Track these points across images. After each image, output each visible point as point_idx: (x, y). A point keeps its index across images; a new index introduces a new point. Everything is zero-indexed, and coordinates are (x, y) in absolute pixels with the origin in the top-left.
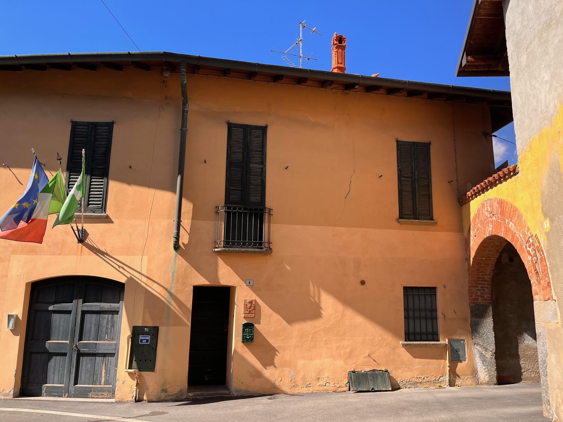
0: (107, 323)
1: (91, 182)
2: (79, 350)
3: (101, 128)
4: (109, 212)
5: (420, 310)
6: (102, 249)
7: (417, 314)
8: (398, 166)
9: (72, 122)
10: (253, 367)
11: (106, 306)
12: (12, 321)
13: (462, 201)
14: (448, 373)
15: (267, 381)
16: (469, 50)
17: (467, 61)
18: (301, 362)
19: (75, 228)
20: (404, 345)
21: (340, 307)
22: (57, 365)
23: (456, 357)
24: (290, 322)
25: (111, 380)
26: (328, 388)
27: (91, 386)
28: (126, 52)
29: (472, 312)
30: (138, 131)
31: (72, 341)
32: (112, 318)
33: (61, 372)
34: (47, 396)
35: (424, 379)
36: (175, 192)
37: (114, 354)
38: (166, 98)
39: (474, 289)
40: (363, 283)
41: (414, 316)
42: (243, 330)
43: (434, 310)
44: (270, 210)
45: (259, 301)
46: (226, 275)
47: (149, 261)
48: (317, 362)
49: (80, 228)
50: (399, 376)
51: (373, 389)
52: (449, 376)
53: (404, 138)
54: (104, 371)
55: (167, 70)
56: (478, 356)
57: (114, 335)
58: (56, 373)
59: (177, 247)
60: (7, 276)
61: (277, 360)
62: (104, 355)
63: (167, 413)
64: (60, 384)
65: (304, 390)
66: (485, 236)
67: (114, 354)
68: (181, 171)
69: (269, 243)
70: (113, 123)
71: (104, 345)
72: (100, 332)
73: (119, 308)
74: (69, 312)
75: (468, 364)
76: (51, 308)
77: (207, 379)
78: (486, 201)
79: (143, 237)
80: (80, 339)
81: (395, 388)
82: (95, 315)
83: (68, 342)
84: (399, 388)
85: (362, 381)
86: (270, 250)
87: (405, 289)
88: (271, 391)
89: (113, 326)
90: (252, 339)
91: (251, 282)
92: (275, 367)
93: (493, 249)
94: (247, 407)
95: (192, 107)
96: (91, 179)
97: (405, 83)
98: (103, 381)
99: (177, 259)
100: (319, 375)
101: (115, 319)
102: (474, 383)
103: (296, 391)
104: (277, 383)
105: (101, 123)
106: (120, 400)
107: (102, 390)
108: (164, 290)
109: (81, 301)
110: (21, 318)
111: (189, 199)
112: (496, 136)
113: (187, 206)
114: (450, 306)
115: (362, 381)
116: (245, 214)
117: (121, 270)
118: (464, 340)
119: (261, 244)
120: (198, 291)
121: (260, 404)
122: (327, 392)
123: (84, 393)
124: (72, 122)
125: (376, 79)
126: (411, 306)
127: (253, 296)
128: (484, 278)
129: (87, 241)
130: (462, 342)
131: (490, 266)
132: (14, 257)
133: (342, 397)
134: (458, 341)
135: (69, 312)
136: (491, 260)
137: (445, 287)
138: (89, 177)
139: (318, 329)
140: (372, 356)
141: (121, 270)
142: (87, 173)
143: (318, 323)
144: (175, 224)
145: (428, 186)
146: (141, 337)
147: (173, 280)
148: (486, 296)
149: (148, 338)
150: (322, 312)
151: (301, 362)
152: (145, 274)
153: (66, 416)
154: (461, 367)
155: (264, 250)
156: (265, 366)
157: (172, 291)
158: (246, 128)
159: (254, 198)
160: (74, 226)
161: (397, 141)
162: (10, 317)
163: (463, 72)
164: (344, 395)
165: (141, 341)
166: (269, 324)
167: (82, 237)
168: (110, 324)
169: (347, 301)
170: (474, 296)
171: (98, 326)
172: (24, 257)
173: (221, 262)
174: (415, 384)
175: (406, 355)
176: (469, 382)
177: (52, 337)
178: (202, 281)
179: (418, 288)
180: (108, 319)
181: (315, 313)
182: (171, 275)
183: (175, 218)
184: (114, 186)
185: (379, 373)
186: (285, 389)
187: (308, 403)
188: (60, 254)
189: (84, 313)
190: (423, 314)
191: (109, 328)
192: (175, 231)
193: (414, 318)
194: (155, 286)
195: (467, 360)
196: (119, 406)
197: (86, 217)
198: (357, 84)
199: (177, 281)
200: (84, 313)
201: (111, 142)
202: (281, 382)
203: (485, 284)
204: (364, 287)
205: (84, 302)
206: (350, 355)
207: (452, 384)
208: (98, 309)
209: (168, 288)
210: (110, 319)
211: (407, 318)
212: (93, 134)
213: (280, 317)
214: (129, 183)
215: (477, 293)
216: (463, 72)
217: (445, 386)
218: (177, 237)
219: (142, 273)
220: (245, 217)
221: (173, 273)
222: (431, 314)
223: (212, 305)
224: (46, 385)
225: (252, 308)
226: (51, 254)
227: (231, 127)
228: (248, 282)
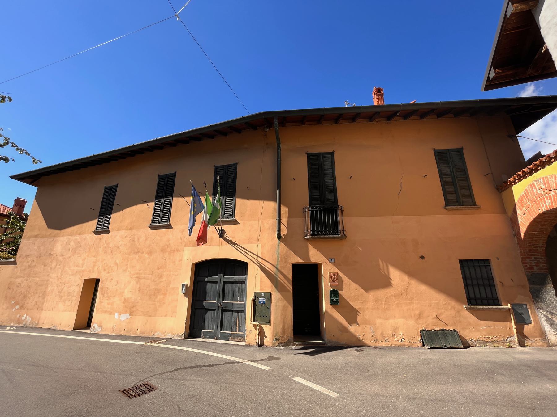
2: (222, 308)
4: (237, 217)
5: (477, 279)
7: (475, 282)
8: (438, 168)
10: (341, 324)
11: (237, 278)
13: (502, 187)
14: (516, 335)
15: (353, 335)
16: (495, 64)
17: (496, 73)
18: (378, 321)
19: (217, 229)
20: (468, 309)
21: (406, 278)
22: (210, 317)
23: (521, 321)
24: (367, 290)
25: (242, 329)
26: (404, 343)
28: (241, 117)
29: (529, 280)
30: (253, 166)
31: (218, 301)
32: (242, 286)
34: (205, 337)
35: (492, 338)
36: (276, 201)
38: (267, 144)
39: (528, 260)
40: (422, 258)
41: (472, 283)
42: (331, 295)
43: (490, 278)
44: (342, 207)
45: (341, 274)
46: (315, 255)
47: (262, 247)
48: (391, 321)
49: (220, 228)
50: (469, 335)
51: (445, 346)
52: (518, 337)
53: (437, 148)
55: (267, 127)
56: (543, 319)
57: (243, 299)
59: (279, 237)
61: (359, 319)
62: (238, 311)
63: (279, 359)
65: (384, 344)
66: (540, 212)
68: (279, 187)
69: (344, 231)
70: (237, 164)
71: (237, 304)
74: (216, 282)
75: (534, 326)
76: (206, 280)
77: (307, 331)
78: (536, 181)
79: (257, 233)
81: (467, 346)
84: (469, 347)
85: (434, 339)
86: (344, 237)
87: (461, 261)
88: (357, 344)
89: (242, 292)
90: (338, 302)
91: (333, 260)
92: (358, 324)
93: (546, 223)
94: (340, 358)
95: (283, 147)
97: (438, 103)
98: (237, 329)
100: (395, 332)
102: (545, 344)
103: (377, 344)
104: (361, 338)
107: (237, 335)
109: (223, 275)
111: (285, 205)
112: (520, 137)
113: (284, 210)
114: (506, 276)
115: (434, 339)
116: (324, 212)
117: (246, 254)
118: (526, 305)
119: (337, 232)
120: (296, 267)
121: (350, 355)
122: (403, 347)
125: (414, 104)
126: (468, 275)
127: (336, 271)
128: (537, 250)
129: (225, 236)
130: (525, 306)
131: (543, 239)
132: (186, 248)
133: (419, 353)
134: (521, 305)
135: (216, 282)
136: (543, 233)
137: (498, 259)
138: (224, 198)
139: (389, 295)
140: (440, 318)
141: (246, 254)
142: (221, 195)
143: (389, 291)
144: (277, 221)
145: (467, 179)
148: (541, 266)
150: (392, 282)
151: (378, 321)
153: (212, 356)
154: (527, 329)
155: (340, 236)
156: (350, 323)
157: (278, 267)
158: (319, 155)
159: (329, 200)
160: (217, 227)
161: (434, 150)
162: (183, 285)
163: (490, 85)
164: (420, 350)
165: (260, 302)
166: (350, 291)
167: (222, 234)
169: (411, 273)
170: (528, 266)
171: (233, 291)
173: (310, 246)
174: (484, 343)
175: (472, 318)
176: (540, 343)
177: (207, 298)
178: (298, 260)
179: (472, 260)
181: (386, 283)
182: (276, 256)
183: (277, 218)
184: (239, 201)
185: (449, 333)
186: (368, 342)
187: (392, 358)
190: (481, 282)
192: (277, 226)
193: (473, 286)
195: (533, 322)
196: (248, 349)
197: (223, 222)
198: (398, 111)
199: (281, 260)
200: (225, 283)
202: (364, 337)
203: (538, 255)
204: (424, 261)
206: (420, 316)
207: (522, 344)
211: (466, 285)
213: (357, 286)
214: (248, 198)
215: (531, 263)
216: (490, 85)
217: (515, 346)
218: (279, 230)
220: (323, 214)
221: (278, 254)
222: (490, 282)
223: (305, 279)
225: (335, 279)
227: (309, 155)
228: (330, 259)
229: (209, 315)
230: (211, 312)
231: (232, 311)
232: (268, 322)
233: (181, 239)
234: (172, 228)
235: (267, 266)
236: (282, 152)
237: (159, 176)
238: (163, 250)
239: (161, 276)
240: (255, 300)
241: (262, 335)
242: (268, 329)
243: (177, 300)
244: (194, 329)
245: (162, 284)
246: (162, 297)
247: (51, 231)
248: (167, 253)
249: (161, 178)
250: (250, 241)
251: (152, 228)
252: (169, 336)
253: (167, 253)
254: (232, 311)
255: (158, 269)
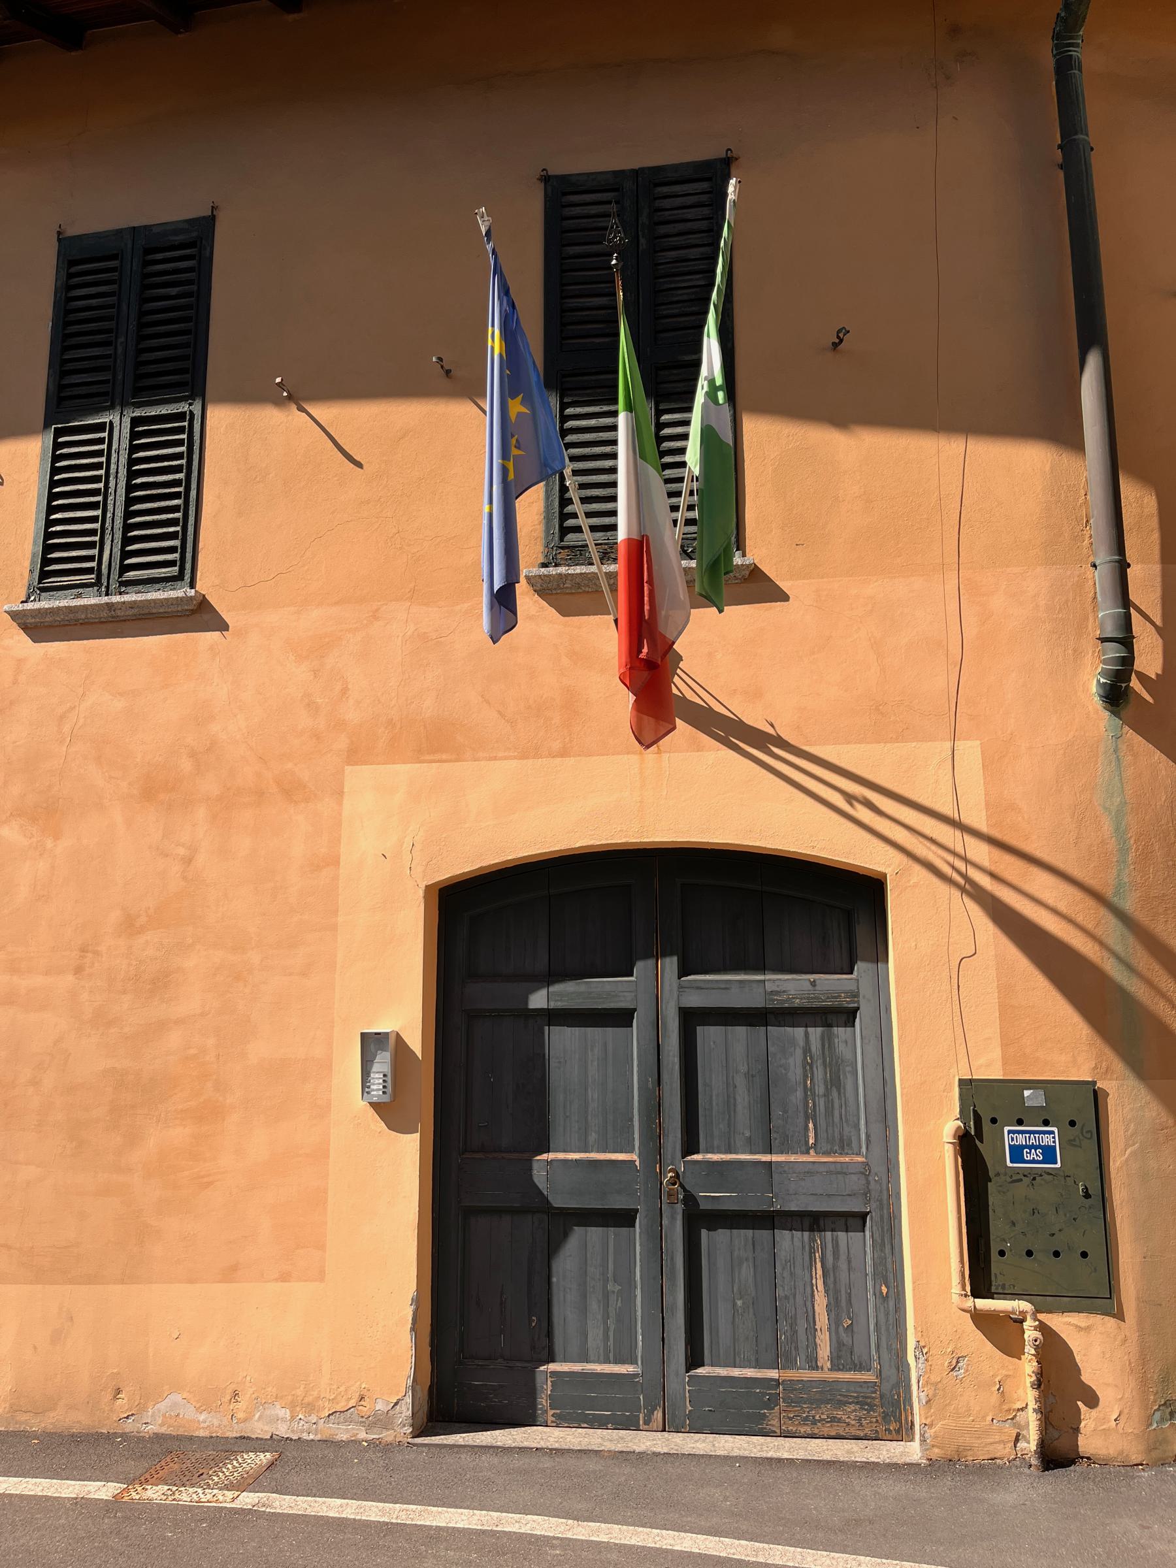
0: (808, 1067)
1: (660, 426)
2: (690, 1200)
3: (677, 189)
6: (754, 718)
9: (546, 179)
11: (792, 987)
12: (382, 1064)
27: (773, 1374)
32: (828, 1042)
33: (615, 1303)
34: (566, 1419)
36: (1073, 441)
37: (863, 1216)
47: (992, 764)
54: (821, 1302)
58: (594, 1305)
59: (1115, 695)
60: (335, 861)
62: (814, 1221)
64: (618, 1361)
67: (863, 1216)
71: (809, 1171)
72: (777, 1112)
73: (855, 995)
74: (622, 1018)
76: (538, 1000)
80: (690, 1145)
82: (741, 1031)
83: (634, 1157)
89: (835, 1082)
96: (563, 406)
98: (824, 1351)
99: (1123, 747)
101: (842, 1049)
105: (676, 167)
106: (950, 1452)
107: (829, 1395)
108: (1090, 902)
109: (670, 965)
110: (415, 1042)
111: (1144, 477)
113: (1139, 502)
123: (743, 1412)
124: (546, 179)
132: (359, 778)
135: (622, 1018)
146: (1010, 1135)
147: (1123, 851)
149: (1047, 1140)
152: (983, 827)
157: (1129, 904)
162: (371, 1043)
165: (1017, 1153)
168: (819, 1073)
171: (766, 1083)
172: (403, 772)
177: (557, 1134)
180: (807, 1050)
182: (1107, 826)
188: (564, 753)
189: (691, 1019)
191: (820, 1089)
194: (1042, 884)
200: (691, 1019)
201: (1099, 287)
205: (684, 971)
208: (754, 1000)
209: (1109, 893)
210: (815, 1046)
212: (644, 219)
214: (842, 417)
219: (966, 819)
224: (552, 1367)
226: (524, 756)
229: (580, 1256)
230: (594, 1234)
231: (768, 1220)
232: (1102, 1297)
233: (312, 707)
234: (222, 626)
235: (1048, 903)
236: (1097, 111)
237: (64, 242)
238: (158, 789)
239: (159, 983)
240: (968, 1146)
241: (1060, 1386)
242: (1098, 1347)
243: (321, 1154)
244: (478, 1359)
245: (174, 1039)
246: (180, 1134)
247: (421, 893)
248: (201, 813)
249: (85, 265)
250: (885, 720)
251: (38, 627)
252: (278, 1421)
253: (201, 813)
254: (768, 1220)
255: (130, 926)
